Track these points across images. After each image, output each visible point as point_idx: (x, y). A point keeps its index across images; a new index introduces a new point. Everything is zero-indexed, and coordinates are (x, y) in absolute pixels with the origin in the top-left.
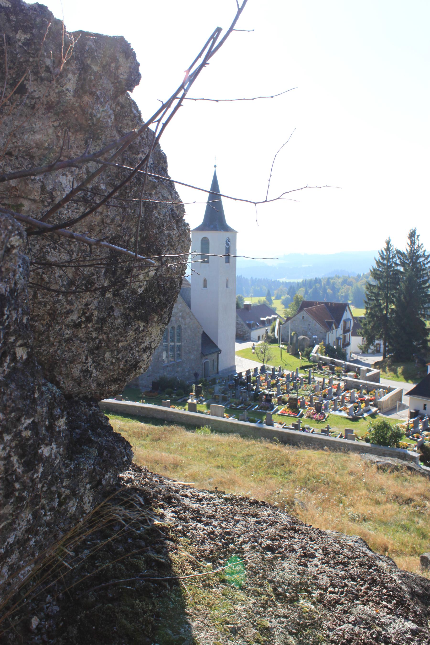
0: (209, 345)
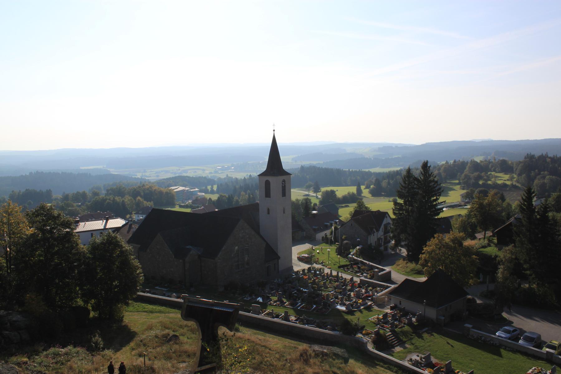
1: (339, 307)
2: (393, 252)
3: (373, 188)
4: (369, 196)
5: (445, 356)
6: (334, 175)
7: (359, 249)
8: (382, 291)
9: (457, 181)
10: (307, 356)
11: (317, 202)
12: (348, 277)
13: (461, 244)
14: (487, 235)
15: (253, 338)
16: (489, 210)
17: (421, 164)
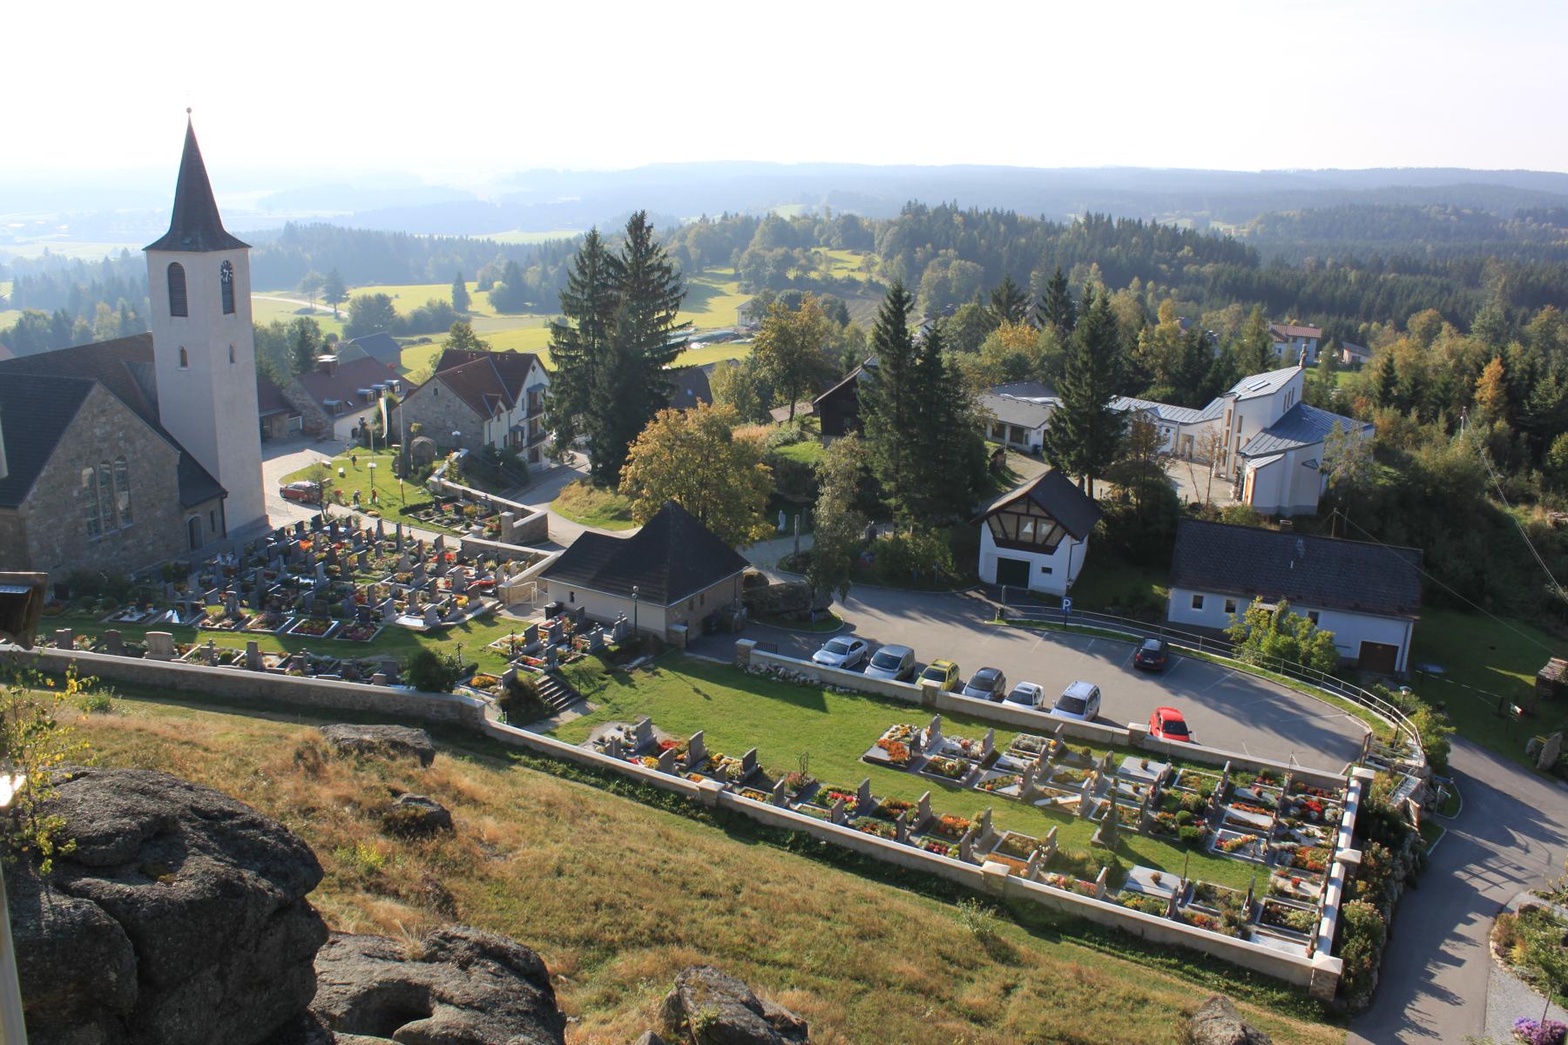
0: (199, 483)
1: (404, 620)
2: (554, 466)
3: (502, 289)
4: (490, 310)
5: (689, 722)
6: (392, 254)
7: (458, 459)
8: (523, 569)
9: (731, 271)
10: (316, 758)
11: (338, 330)
12: (427, 537)
13: (727, 436)
14: (798, 412)
15: (154, 725)
16: (803, 346)
17: (626, 221)
